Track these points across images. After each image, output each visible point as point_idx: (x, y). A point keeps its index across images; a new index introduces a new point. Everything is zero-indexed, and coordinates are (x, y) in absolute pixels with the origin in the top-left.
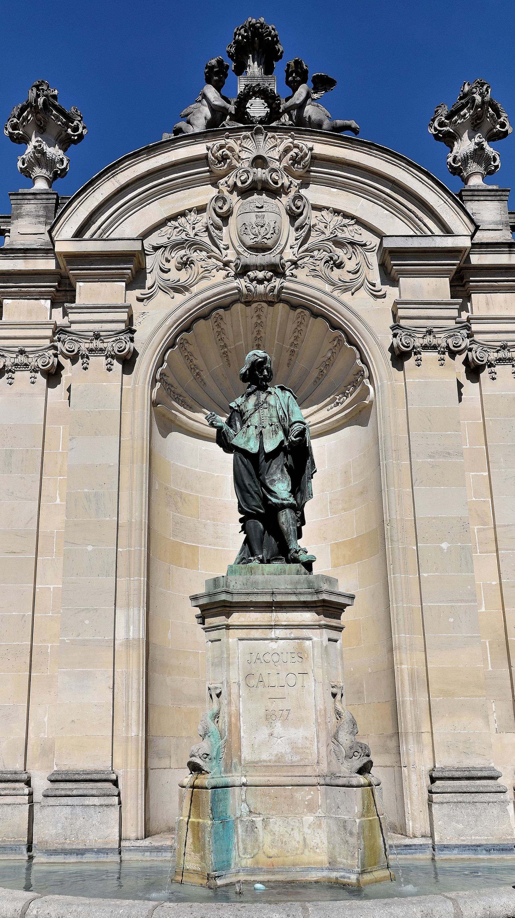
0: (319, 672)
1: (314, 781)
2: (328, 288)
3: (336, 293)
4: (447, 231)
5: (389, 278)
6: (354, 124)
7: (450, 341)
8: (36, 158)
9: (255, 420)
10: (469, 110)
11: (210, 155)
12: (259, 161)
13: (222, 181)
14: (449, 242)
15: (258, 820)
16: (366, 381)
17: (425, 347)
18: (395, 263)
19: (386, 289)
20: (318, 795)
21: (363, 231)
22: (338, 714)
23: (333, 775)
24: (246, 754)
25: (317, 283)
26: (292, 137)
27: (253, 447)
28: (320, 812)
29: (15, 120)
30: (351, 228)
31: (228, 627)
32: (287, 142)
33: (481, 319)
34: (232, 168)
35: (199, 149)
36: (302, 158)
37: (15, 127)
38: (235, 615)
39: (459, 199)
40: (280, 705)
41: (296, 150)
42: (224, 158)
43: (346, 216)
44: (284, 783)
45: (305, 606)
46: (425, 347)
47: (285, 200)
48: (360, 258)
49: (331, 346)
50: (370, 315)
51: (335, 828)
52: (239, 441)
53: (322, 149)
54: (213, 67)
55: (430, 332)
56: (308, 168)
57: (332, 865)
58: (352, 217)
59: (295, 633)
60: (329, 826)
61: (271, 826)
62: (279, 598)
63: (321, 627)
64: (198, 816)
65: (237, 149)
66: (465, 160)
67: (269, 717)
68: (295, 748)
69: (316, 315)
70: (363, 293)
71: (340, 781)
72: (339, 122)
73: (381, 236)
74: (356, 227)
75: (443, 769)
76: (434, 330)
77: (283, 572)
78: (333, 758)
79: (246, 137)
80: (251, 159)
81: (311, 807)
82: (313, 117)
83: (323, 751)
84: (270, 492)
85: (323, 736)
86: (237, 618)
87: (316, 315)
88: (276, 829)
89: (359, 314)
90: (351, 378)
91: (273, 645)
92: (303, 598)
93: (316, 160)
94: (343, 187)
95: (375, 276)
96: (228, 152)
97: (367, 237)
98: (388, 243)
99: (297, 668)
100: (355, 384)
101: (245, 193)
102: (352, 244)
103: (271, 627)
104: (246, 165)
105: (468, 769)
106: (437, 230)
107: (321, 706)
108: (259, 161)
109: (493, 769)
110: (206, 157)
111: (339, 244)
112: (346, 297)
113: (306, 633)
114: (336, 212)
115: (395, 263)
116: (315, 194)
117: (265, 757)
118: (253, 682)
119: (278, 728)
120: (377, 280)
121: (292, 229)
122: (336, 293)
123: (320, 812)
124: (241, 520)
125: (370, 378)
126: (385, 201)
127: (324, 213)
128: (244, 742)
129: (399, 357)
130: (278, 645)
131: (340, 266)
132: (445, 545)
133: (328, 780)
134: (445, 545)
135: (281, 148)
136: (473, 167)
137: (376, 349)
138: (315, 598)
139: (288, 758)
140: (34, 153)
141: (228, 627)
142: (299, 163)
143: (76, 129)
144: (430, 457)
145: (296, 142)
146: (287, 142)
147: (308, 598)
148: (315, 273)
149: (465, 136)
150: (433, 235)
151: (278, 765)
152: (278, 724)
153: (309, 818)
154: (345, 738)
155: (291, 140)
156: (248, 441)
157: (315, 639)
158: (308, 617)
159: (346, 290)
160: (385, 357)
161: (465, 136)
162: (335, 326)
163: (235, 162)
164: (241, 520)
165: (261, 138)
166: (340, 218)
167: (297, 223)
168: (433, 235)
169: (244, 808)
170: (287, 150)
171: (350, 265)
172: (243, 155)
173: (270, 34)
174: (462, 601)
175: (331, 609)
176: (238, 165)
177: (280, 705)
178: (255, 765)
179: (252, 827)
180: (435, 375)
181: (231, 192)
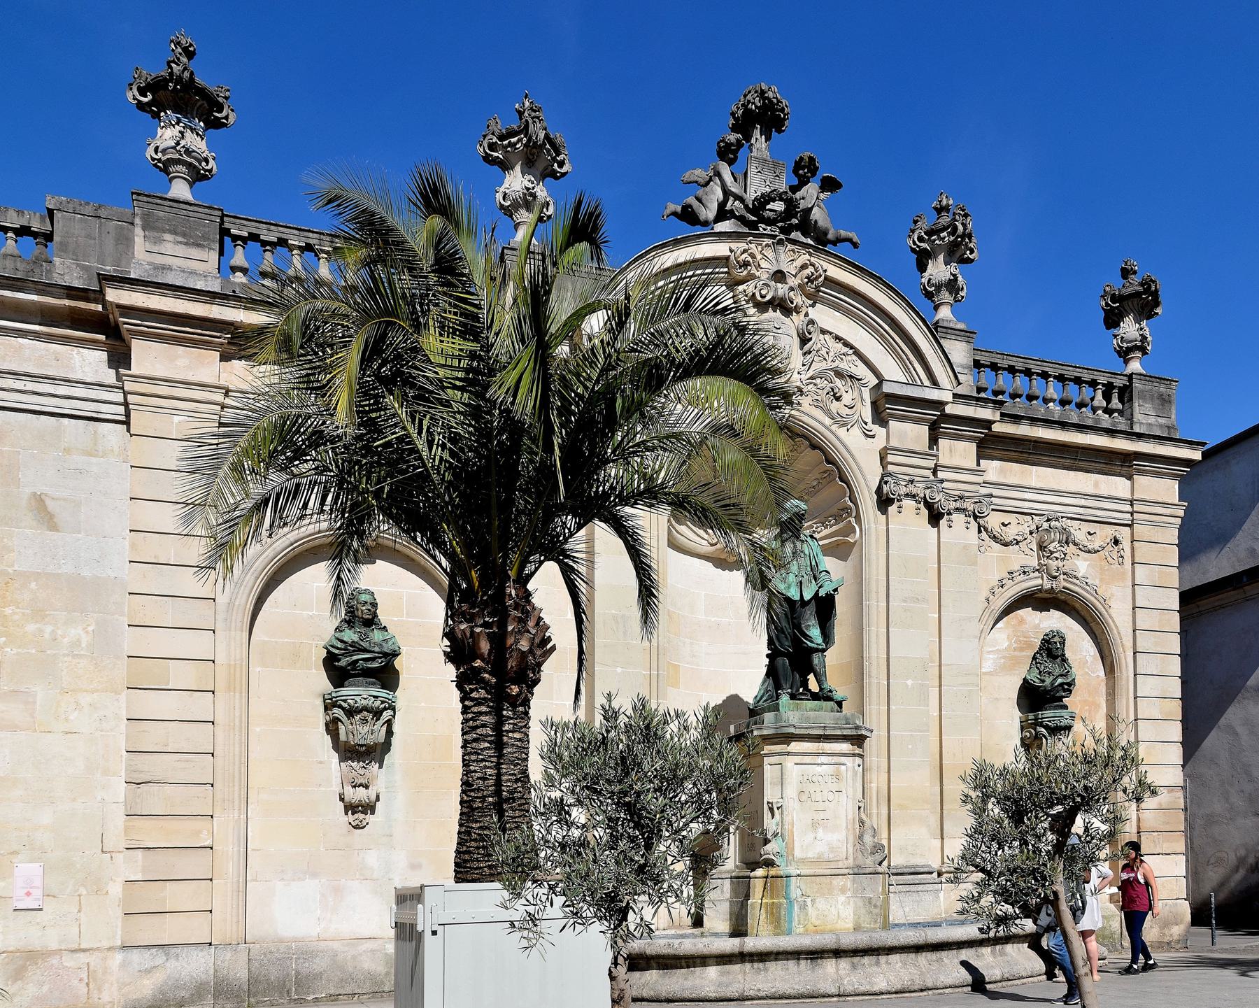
0: (850, 790)
1: (846, 871)
2: (828, 421)
3: (834, 428)
4: (935, 383)
5: (880, 418)
6: (856, 239)
7: (927, 492)
8: (525, 200)
9: (794, 567)
10: (949, 234)
11: (732, 258)
12: (779, 276)
13: (741, 288)
14: (934, 395)
15: (808, 900)
16: (852, 520)
17: (907, 495)
18: (886, 406)
19: (876, 429)
20: (848, 882)
21: (859, 363)
22: (862, 822)
23: (859, 867)
24: (798, 853)
25: (819, 414)
26: (810, 254)
27: (794, 594)
28: (849, 894)
29: (495, 140)
30: (849, 358)
31: (789, 754)
32: (804, 258)
33: (948, 468)
34: (751, 277)
35: (720, 249)
36: (817, 278)
37: (492, 147)
38: (793, 744)
39: (936, 331)
40: (822, 815)
41: (811, 269)
42: (746, 264)
43: (846, 344)
44: (823, 874)
45: (844, 738)
46: (907, 495)
47: (798, 320)
48: (856, 394)
49: (819, 476)
50: (861, 450)
51: (860, 904)
52: (778, 585)
53: (835, 272)
54: (732, 144)
55: (912, 482)
56: (818, 289)
57: (857, 929)
58: (852, 347)
59: (835, 759)
60: (855, 903)
61: (817, 905)
62: (828, 732)
63: (854, 755)
64: (772, 898)
65: (759, 257)
66: (939, 287)
67: (815, 825)
68: (832, 849)
69: (814, 446)
70: (856, 431)
71: (867, 871)
72: (843, 233)
73: (881, 380)
74: (854, 357)
75: (896, 867)
76: (917, 479)
77: (821, 709)
78: (859, 855)
79: (767, 245)
80: (771, 272)
81: (843, 890)
82: (820, 223)
83: (851, 850)
84: (806, 636)
85: (851, 838)
86: (795, 746)
87: (814, 446)
88: (820, 906)
89: (854, 452)
90: (834, 510)
91: (818, 768)
92: (845, 733)
93: (831, 283)
94: (847, 313)
95: (867, 414)
96: (749, 259)
97: (861, 370)
98: (887, 388)
99: (835, 787)
100: (838, 518)
101: (762, 307)
102: (851, 377)
103: (818, 754)
104: (765, 276)
105: (913, 867)
106: (927, 383)
107: (850, 817)
108: (779, 276)
109: (929, 866)
110: (727, 258)
111: (839, 374)
112: (842, 432)
113: (843, 760)
114: (838, 338)
115: (886, 406)
116: (824, 316)
117: (810, 855)
118: (804, 797)
119: (820, 833)
120: (869, 419)
121: (801, 352)
122: (834, 428)
123: (849, 894)
124: (768, 656)
125: (858, 518)
126: (882, 336)
127: (827, 337)
128: (797, 844)
129: (884, 502)
130: (823, 770)
131: (838, 399)
132: (909, 682)
133: (856, 871)
134: (909, 682)
135: (798, 263)
136: (945, 296)
137: (866, 491)
138: (854, 733)
139: (826, 855)
140: (524, 194)
141: (789, 754)
142: (812, 282)
143: (561, 164)
144: (904, 601)
145: (813, 259)
146: (804, 258)
147: (849, 732)
148: (817, 404)
149: (941, 258)
150: (922, 385)
151: (818, 861)
152: (820, 830)
153: (842, 898)
154: (868, 839)
155: (807, 256)
156: (789, 587)
157: (849, 764)
158: (845, 747)
159: (842, 426)
160: (872, 498)
161: (941, 258)
162: (830, 461)
163: (754, 271)
164: (768, 656)
165: (781, 248)
166: (840, 345)
167: (806, 348)
168: (922, 385)
169: (799, 892)
170: (804, 267)
171: (847, 399)
172: (764, 264)
173: (782, 110)
174: (919, 731)
175: (858, 740)
176: (757, 274)
177: (822, 815)
178: (803, 861)
179: (804, 906)
180: (908, 519)
181: (747, 302)
